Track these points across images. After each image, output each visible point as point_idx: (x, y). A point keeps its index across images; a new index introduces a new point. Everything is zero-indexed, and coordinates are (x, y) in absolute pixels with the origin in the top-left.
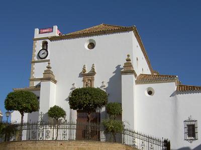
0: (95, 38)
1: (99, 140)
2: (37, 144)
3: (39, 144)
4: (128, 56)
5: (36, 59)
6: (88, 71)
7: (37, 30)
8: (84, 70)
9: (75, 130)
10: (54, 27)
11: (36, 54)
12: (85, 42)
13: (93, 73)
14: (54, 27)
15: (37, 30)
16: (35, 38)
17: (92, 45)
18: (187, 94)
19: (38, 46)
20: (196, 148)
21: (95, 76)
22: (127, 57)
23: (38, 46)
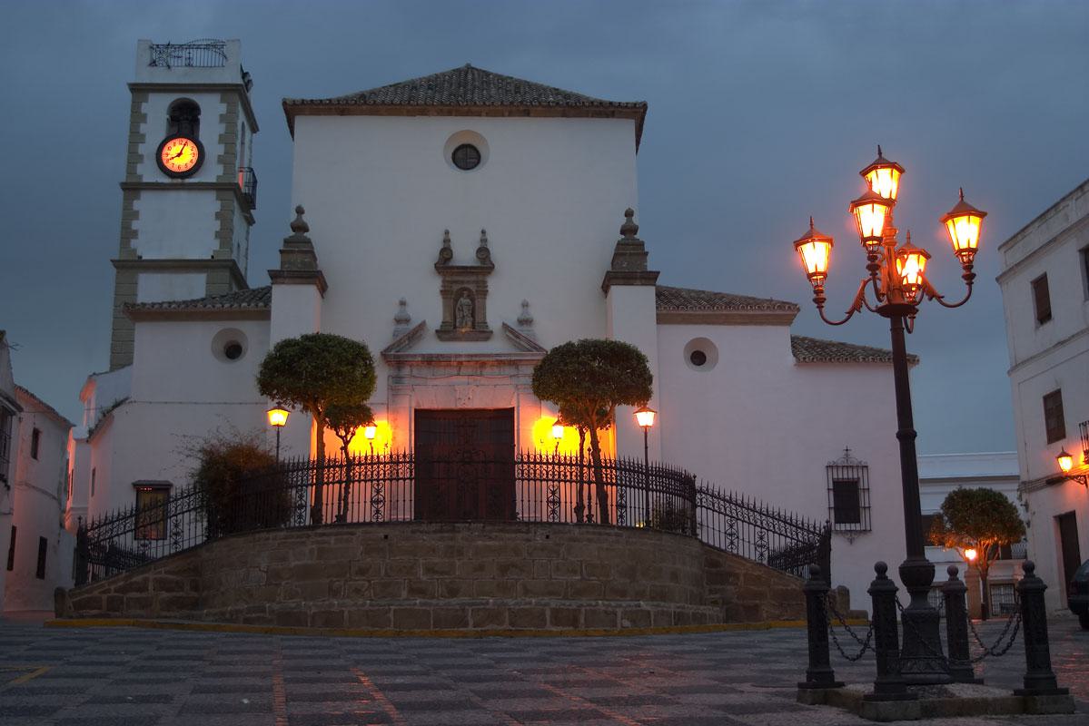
2: (459, 536)
6: (465, 255)
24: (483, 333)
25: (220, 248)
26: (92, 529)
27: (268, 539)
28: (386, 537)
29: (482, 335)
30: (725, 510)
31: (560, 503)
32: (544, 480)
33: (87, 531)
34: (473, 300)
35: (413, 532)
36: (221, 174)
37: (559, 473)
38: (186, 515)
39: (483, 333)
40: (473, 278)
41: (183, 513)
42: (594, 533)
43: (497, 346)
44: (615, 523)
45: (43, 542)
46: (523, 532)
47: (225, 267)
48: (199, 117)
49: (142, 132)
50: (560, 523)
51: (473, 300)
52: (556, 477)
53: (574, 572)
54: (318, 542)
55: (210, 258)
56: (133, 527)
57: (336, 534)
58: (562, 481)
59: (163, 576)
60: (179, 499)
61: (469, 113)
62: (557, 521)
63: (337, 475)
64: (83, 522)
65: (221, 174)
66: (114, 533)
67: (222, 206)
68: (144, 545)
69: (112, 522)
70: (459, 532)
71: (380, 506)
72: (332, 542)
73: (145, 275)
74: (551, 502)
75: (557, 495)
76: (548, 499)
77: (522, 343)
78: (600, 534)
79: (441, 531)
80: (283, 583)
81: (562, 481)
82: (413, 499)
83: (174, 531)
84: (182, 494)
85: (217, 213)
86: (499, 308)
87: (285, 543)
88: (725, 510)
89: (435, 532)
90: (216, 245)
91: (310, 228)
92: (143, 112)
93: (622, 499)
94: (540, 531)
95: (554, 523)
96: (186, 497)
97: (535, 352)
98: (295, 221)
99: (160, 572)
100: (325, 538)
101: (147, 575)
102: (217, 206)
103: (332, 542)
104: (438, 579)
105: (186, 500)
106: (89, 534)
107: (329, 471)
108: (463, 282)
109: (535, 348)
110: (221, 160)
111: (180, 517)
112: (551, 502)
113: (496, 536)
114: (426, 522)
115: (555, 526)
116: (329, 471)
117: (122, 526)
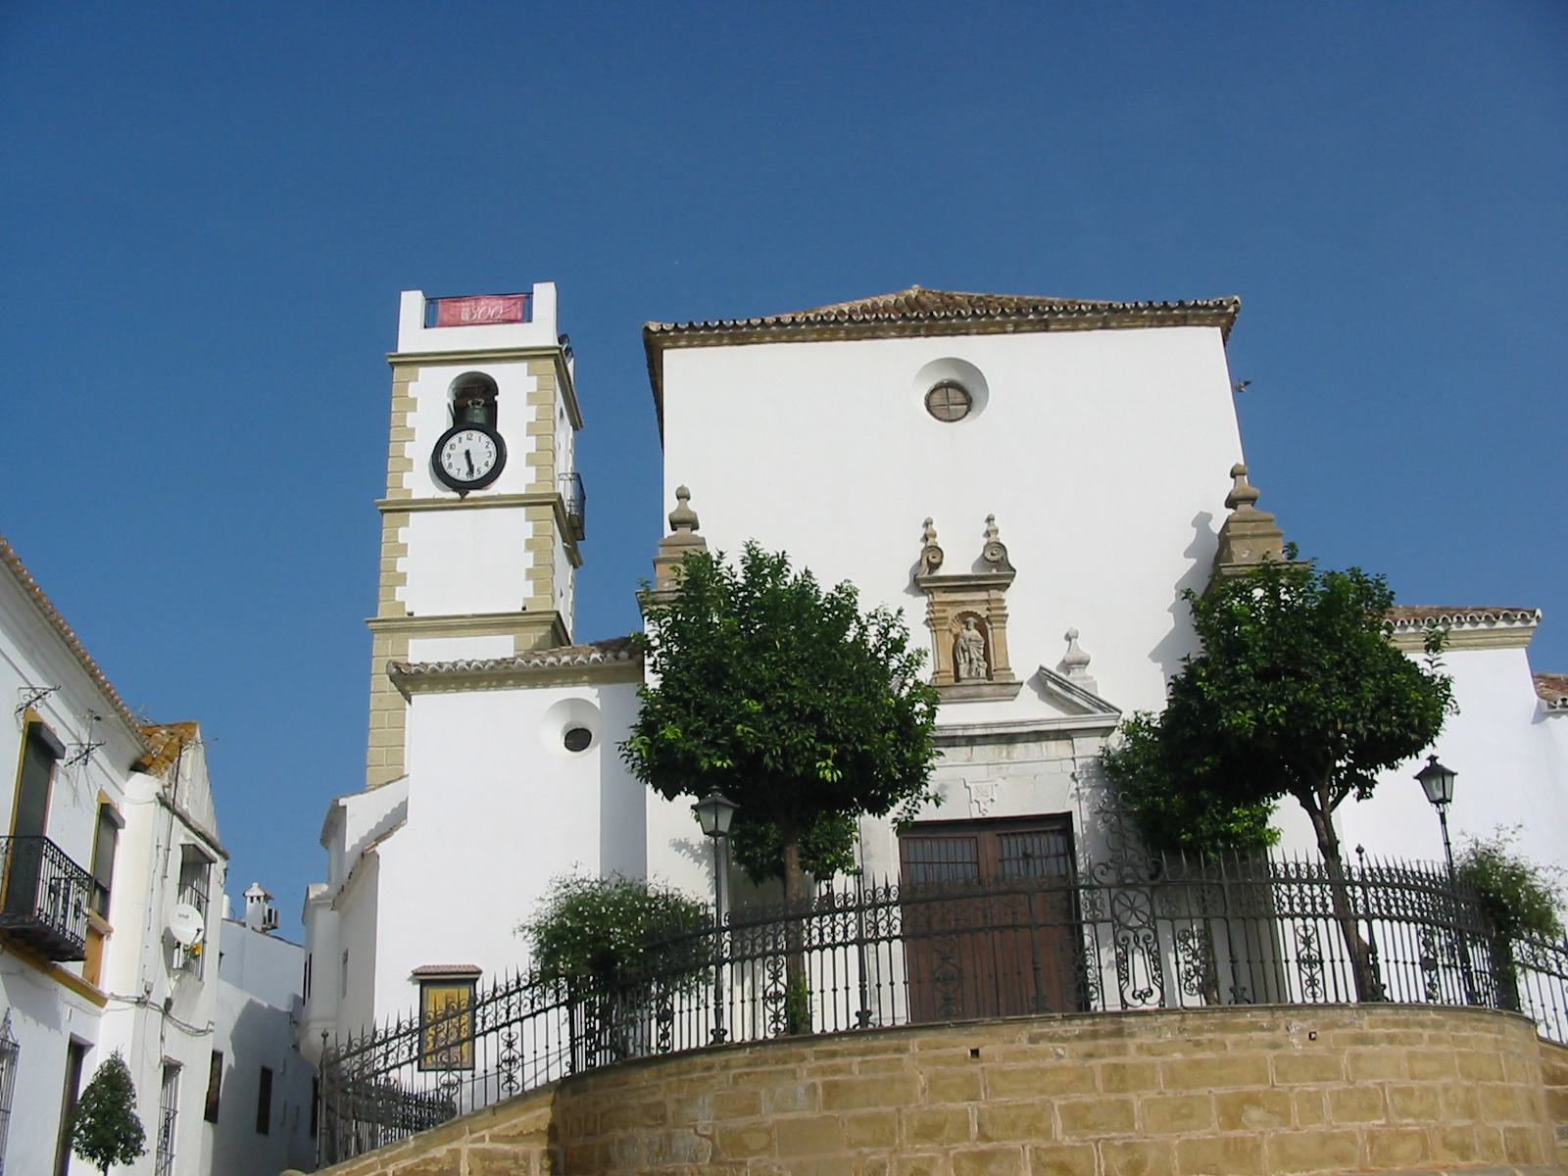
0: (986, 352)
1: (1083, 1006)
2: (1132, 1044)
3: (1147, 1039)
4: (990, 520)
5: (419, 483)
6: (959, 562)
7: (412, 303)
8: (932, 555)
9: (897, 944)
10: (537, 287)
11: (419, 451)
12: (908, 362)
13: (996, 572)
14: (537, 287)
15: (412, 303)
16: (401, 350)
17: (954, 397)
18: (365, 834)
19: (425, 403)
20: (235, 1054)
21: (1012, 598)
22: (985, 527)
23: (425, 403)
24: (1008, 688)
25: (535, 594)
26: (349, 1055)
27: (709, 1068)
28: (975, 1052)
29: (1005, 690)
30: (1560, 967)
31: (1321, 962)
32: (1287, 915)
33: (338, 1060)
34: (984, 632)
35: (1033, 1040)
36: (533, 481)
37: (1313, 898)
38: (528, 1022)
39: (997, 682)
40: (983, 595)
41: (521, 1020)
42: (1396, 1024)
43: (1029, 708)
44: (1298, 1000)
45: (266, 1075)
46: (1262, 1029)
47: (543, 623)
48: (496, 398)
49: (409, 425)
50: (1326, 1006)
51: (984, 632)
52: (1309, 908)
53: (1372, 1110)
54: (823, 1071)
55: (520, 610)
56: (415, 1053)
57: (863, 1053)
58: (1320, 915)
59: (487, 1145)
60: (513, 993)
61: (955, 331)
62: (1321, 1000)
63: (852, 927)
64: (330, 1040)
65: (533, 481)
66: (391, 1063)
67: (536, 528)
68: (449, 1085)
69: (386, 1041)
70: (1132, 1035)
71: (772, 989)
72: (855, 1069)
73: (413, 638)
74: (1304, 961)
75: (1314, 946)
76: (1298, 954)
77: (1076, 699)
78: (1406, 1024)
79: (1094, 1035)
80: (750, 1161)
81: (1320, 915)
82: (1284, 964)
83: (506, 1055)
84: (518, 983)
85: (528, 542)
86: (1028, 642)
87: (747, 1074)
88: (1560, 967)
89: (1079, 1037)
90: (527, 589)
91: (701, 527)
92: (410, 395)
93: (1427, 950)
94: (1296, 1025)
95: (1315, 1006)
96: (526, 988)
97: (1100, 713)
98: (677, 510)
99: (482, 1139)
100: (839, 1061)
101: (455, 1145)
102: (528, 530)
103: (855, 1069)
104: (1097, 1142)
105: (527, 993)
106: (344, 1063)
107: (833, 919)
108: (963, 603)
109: (1100, 707)
110: (531, 460)
111: (516, 1027)
112: (1304, 961)
113: (1210, 1041)
114: (1058, 1015)
115: (1321, 1013)
116: (833, 919)
117: (406, 1049)
